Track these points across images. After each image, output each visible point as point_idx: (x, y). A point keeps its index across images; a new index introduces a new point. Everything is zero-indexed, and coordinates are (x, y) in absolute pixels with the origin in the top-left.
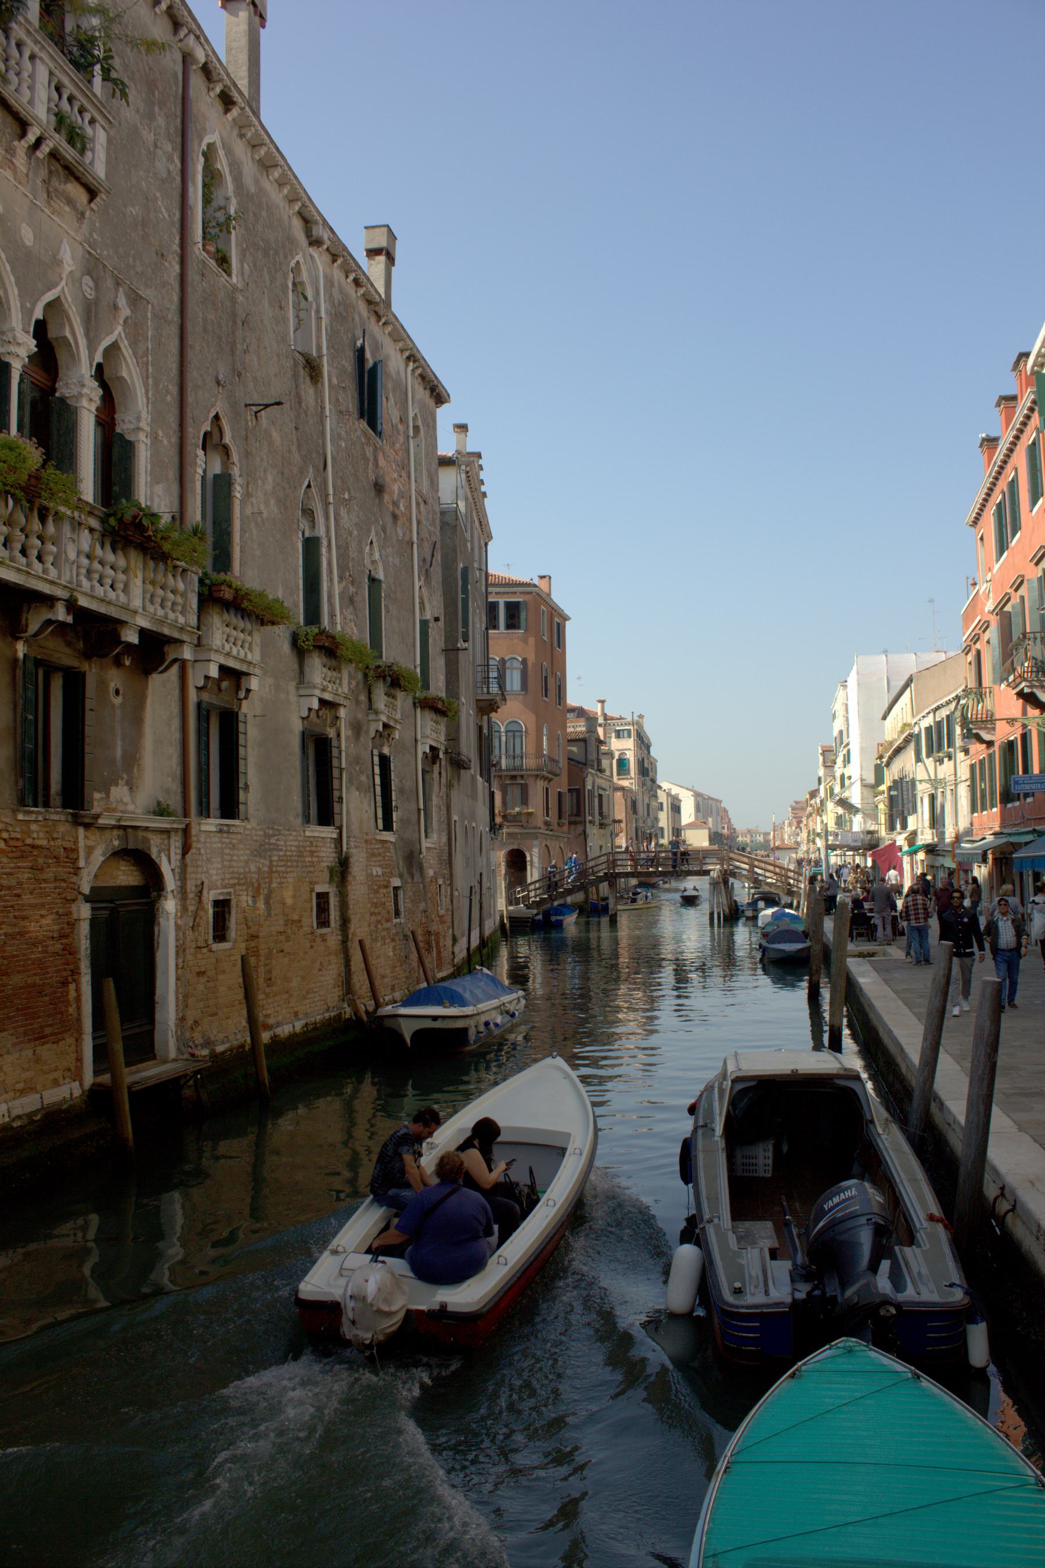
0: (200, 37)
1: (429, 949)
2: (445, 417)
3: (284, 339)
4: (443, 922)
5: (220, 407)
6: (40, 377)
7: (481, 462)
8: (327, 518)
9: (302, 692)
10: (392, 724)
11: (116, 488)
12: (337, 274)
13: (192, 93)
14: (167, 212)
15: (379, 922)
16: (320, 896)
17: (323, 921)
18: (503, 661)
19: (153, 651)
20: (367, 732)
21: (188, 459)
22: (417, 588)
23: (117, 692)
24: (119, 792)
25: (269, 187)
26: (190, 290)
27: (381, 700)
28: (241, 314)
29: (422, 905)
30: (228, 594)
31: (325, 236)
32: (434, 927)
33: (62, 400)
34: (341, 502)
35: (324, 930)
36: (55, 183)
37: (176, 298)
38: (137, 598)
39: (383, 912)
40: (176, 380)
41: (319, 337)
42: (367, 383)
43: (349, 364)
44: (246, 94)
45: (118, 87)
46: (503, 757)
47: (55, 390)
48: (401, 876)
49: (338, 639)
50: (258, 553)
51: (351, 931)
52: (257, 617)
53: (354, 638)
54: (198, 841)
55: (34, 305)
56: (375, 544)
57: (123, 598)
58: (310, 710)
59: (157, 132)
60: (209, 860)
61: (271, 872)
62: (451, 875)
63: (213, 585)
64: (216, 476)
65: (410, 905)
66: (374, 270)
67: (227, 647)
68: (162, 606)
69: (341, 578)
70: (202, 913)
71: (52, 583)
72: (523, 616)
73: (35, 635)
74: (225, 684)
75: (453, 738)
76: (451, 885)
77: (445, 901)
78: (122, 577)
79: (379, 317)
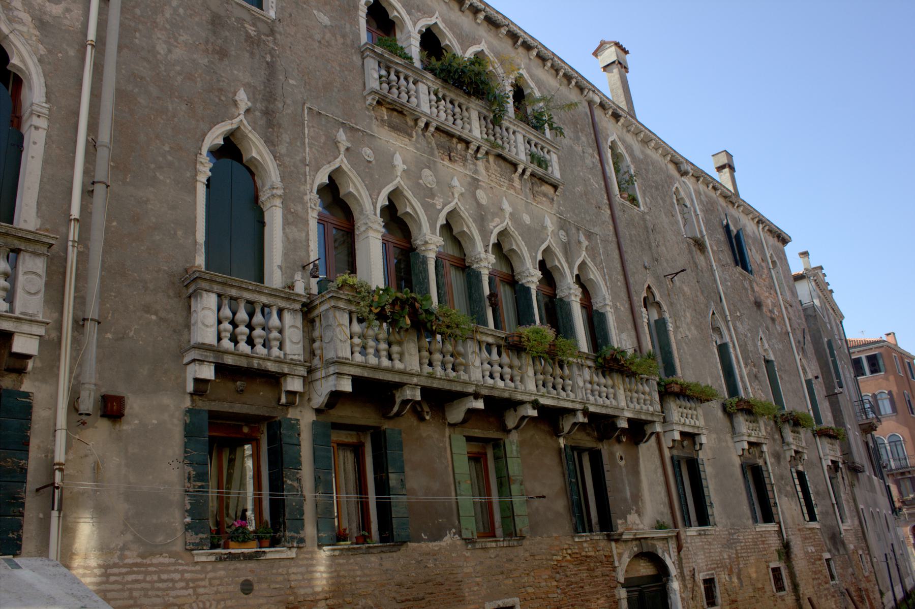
0: (595, 90)
1: (863, 601)
2: (791, 251)
3: (678, 233)
4: (869, 581)
5: (649, 281)
6: (547, 290)
7: (823, 271)
8: (729, 330)
9: (736, 440)
10: (800, 450)
11: (600, 341)
12: (701, 187)
13: (597, 119)
14: (596, 184)
15: (820, 584)
16: (774, 570)
17: (780, 587)
18: (874, 396)
19: (638, 431)
20: (785, 458)
21: (637, 315)
22: (798, 361)
23: (621, 458)
24: (632, 518)
25: (649, 152)
26: (618, 221)
27: (789, 436)
28: (650, 226)
29: (850, 570)
30: (676, 389)
31: (689, 168)
32: (863, 585)
33: (561, 299)
34: (736, 319)
35: (782, 593)
36: (536, 188)
37: (611, 228)
38: (623, 401)
39: (822, 577)
40: (621, 273)
41: (699, 226)
42: (736, 246)
43: (721, 236)
44: (626, 109)
45: (558, 131)
46: (891, 461)
47: (556, 295)
48: (829, 551)
49: (752, 403)
50: (690, 360)
51: (801, 592)
52: (697, 398)
53: (763, 400)
54: (687, 542)
55: (536, 254)
56: (764, 339)
57: (614, 403)
58: (743, 450)
59: (583, 146)
60: (695, 554)
61: (738, 557)
62: (868, 547)
63: (666, 385)
64: (656, 321)
65: (840, 571)
66: (724, 178)
67: (682, 420)
68: (638, 403)
69: (746, 365)
70: (697, 589)
71: (573, 401)
72: (881, 362)
73: (569, 432)
74: (685, 443)
75: (847, 452)
76: (869, 554)
77: (868, 566)
78: (611, 390)
79: (733, 204)
